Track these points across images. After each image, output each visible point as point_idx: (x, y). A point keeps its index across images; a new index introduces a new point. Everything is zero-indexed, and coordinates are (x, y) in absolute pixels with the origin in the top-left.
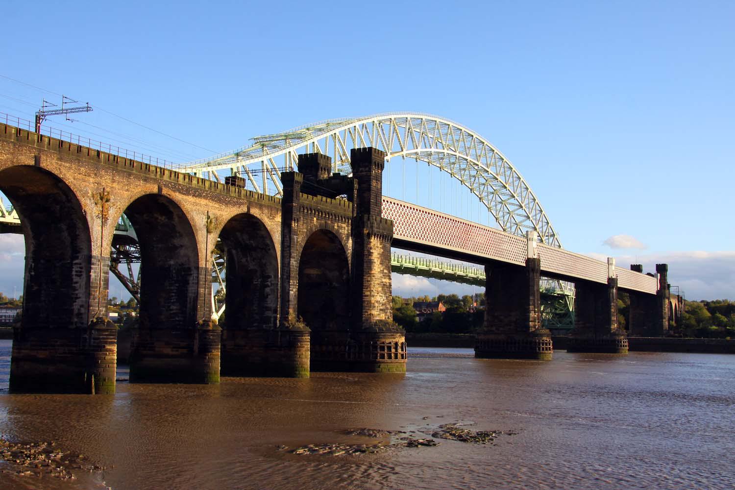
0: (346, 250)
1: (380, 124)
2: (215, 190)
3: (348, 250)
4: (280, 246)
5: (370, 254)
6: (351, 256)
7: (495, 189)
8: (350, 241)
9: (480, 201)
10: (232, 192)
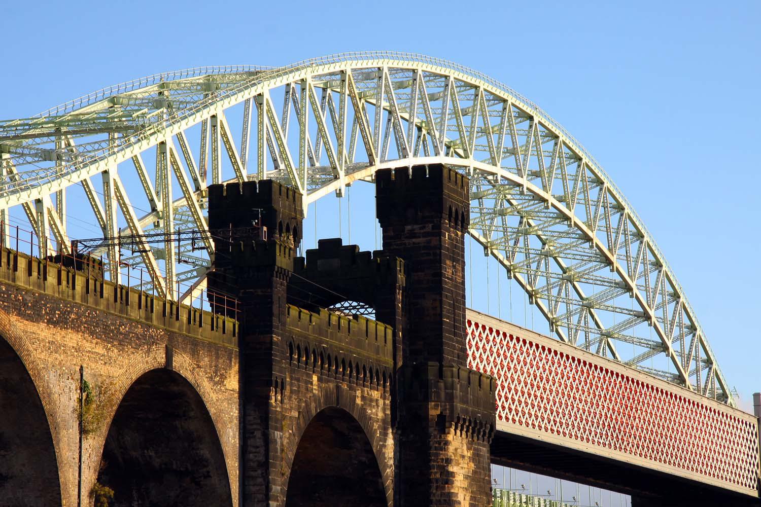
0: (381, 468)
1: (324, 90)
2: (97, 303)
3: (386, 466)
4: (237, 465)
5: (448, 478)
6: (392, 486)
7: (564, 265)
8: (390, 441)
9: (531, 303)
10: (132, 307)
